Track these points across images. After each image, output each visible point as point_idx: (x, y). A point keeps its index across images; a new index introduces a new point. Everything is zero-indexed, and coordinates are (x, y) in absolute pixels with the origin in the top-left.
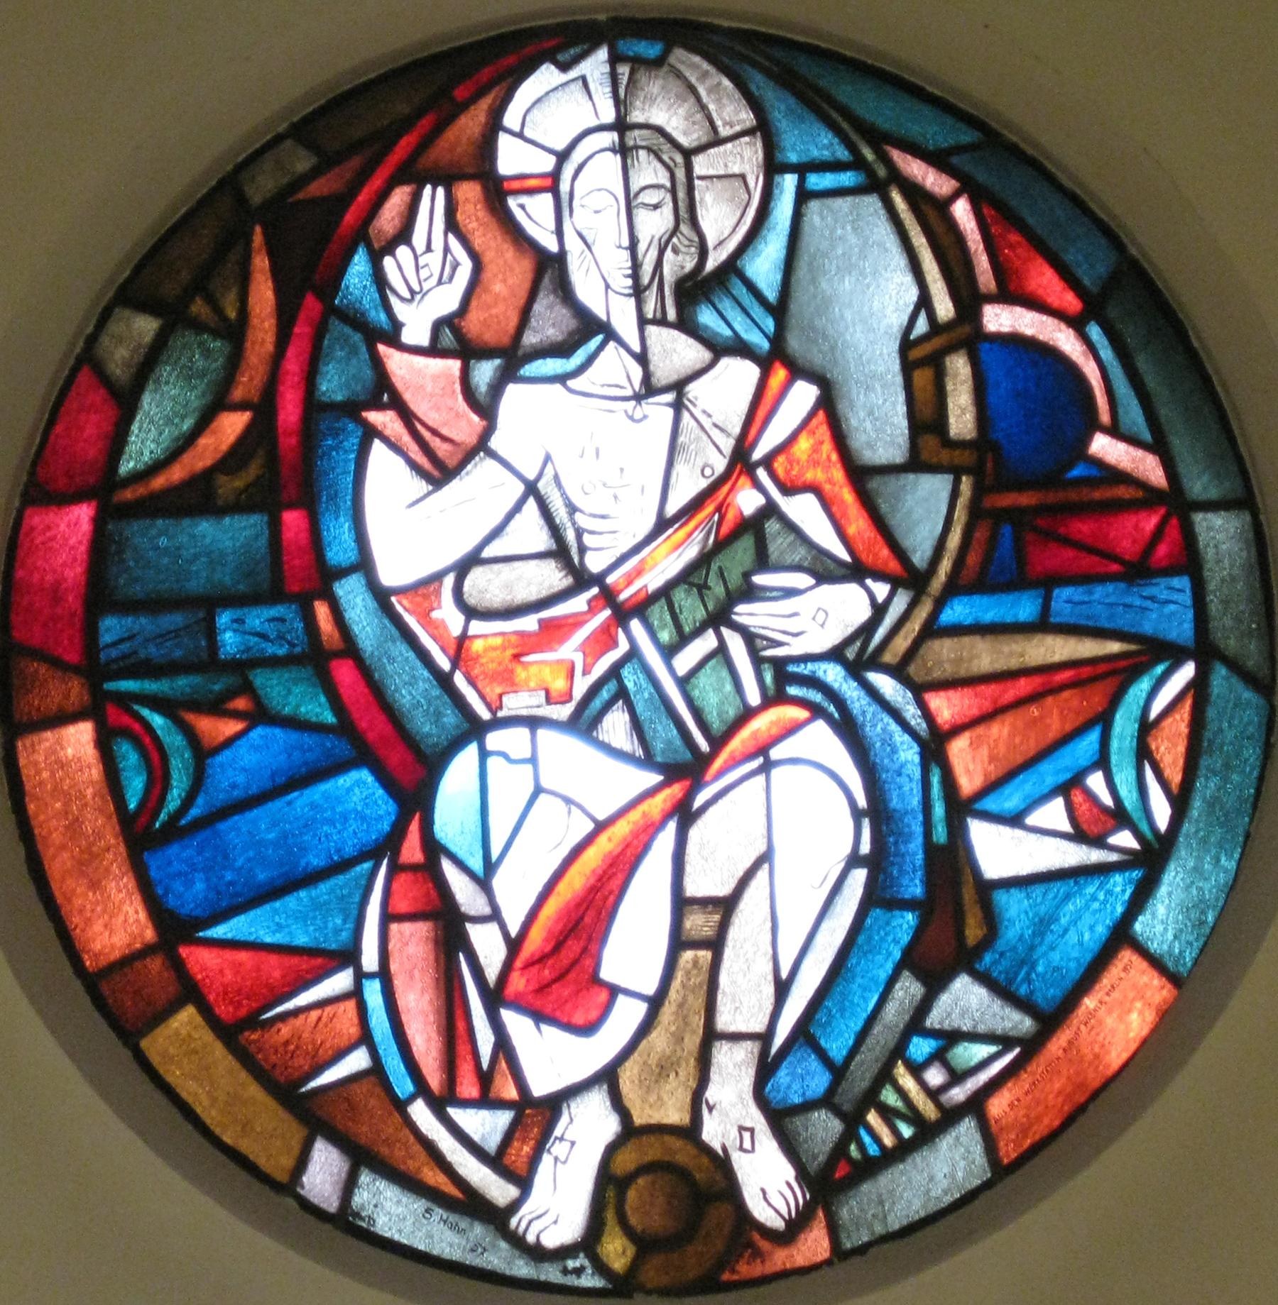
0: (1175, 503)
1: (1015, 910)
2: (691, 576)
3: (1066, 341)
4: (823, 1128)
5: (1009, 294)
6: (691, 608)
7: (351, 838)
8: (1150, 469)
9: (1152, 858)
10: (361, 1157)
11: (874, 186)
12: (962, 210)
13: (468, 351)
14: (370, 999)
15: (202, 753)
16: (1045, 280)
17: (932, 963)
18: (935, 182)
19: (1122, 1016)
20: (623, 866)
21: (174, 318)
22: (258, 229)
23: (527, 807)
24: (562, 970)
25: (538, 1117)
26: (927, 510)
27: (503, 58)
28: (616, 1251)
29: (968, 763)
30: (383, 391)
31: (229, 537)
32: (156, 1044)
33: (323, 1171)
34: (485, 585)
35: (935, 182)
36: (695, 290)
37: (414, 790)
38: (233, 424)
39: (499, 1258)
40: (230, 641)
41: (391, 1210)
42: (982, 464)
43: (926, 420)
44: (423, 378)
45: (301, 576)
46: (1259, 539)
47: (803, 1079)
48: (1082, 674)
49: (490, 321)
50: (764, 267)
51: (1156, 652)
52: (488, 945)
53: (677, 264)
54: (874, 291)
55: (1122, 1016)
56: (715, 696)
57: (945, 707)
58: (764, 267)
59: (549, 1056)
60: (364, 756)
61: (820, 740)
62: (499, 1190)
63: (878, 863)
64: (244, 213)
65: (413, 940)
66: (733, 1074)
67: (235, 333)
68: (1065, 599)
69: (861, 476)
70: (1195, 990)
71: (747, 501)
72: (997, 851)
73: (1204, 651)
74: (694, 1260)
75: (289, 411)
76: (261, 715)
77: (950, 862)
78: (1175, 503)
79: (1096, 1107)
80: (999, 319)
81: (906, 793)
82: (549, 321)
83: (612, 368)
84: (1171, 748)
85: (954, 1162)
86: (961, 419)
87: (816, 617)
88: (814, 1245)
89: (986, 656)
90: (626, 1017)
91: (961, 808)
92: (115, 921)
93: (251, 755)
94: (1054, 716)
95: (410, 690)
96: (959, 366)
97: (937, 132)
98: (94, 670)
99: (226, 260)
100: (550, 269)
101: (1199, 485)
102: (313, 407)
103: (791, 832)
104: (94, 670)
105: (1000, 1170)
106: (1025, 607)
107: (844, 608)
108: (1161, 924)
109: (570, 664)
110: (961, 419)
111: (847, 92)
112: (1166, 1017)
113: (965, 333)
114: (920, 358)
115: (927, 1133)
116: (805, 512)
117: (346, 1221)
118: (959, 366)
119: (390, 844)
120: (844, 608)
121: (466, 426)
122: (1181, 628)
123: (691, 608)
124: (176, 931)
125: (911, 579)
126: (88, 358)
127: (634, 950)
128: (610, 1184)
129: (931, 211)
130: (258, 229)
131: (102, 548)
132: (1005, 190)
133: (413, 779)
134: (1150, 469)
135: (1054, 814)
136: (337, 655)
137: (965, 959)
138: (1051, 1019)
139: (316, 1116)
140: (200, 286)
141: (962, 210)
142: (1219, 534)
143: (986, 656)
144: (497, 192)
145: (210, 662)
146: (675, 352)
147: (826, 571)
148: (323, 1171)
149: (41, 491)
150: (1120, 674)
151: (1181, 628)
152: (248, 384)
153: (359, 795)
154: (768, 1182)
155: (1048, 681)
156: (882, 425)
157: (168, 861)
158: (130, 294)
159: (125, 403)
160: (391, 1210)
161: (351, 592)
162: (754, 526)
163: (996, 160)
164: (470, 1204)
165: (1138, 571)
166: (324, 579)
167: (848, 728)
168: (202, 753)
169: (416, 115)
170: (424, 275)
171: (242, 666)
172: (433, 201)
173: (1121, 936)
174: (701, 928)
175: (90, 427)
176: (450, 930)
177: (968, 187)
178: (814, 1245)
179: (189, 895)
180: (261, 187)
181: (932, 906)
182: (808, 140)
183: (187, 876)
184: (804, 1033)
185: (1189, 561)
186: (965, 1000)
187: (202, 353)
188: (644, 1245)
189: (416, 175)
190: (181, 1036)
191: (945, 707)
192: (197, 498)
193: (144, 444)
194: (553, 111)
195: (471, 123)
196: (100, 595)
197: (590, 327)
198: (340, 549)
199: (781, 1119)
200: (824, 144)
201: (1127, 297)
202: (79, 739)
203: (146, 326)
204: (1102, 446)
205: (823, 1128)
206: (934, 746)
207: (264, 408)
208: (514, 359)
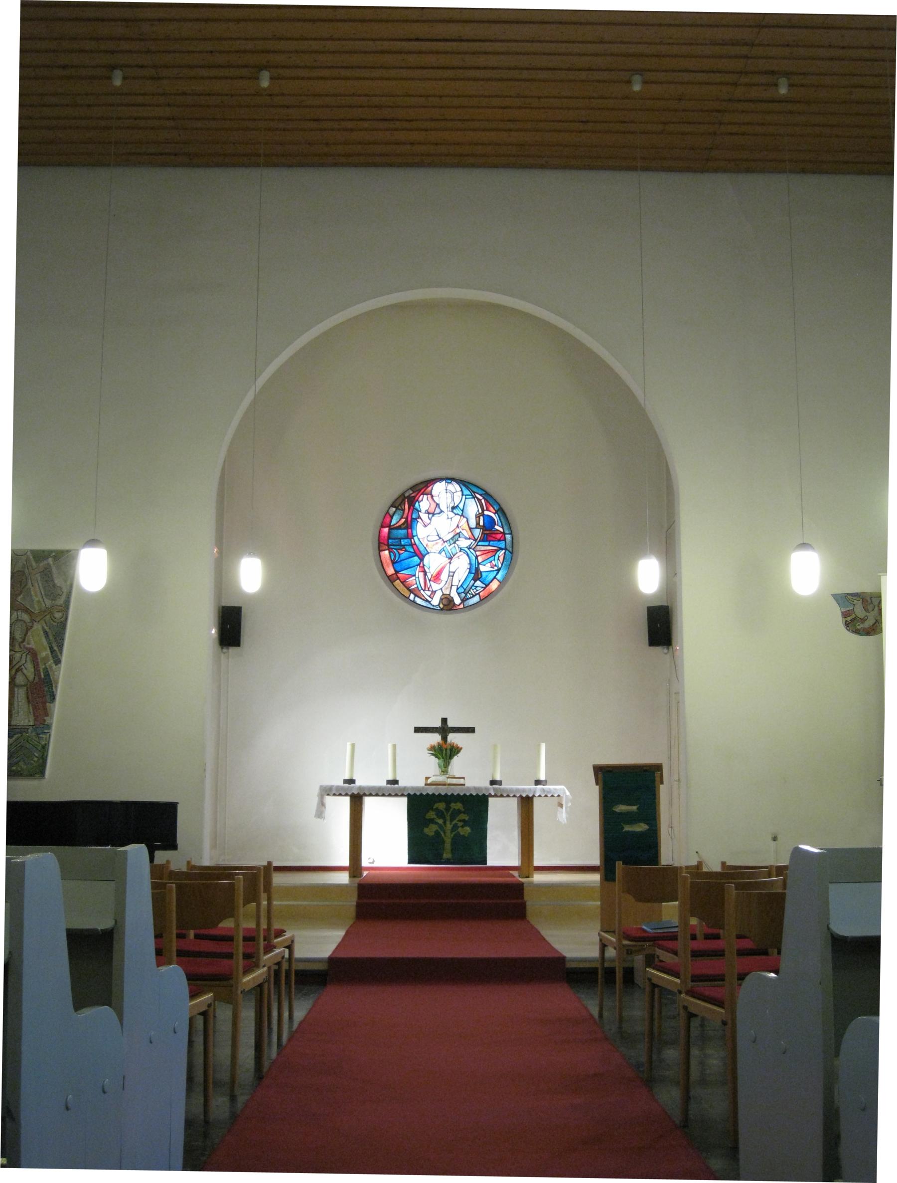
0: (504, 533)
1: (484, 574)
2: (452, 539)
3: (493, 515)
4: (463, 595)
5: (488, 510)
6: (452, 542)
7: (415, 564)
8: (501, 530)
9: (499, 570)
10: (416, 595)
11: (474, 497)
12: (483, 501)
13: (429, 513)
14: (417, 580)
15: (400, 554)
16: (491, 509)
17: (475, 579)
18: (480, 497)
19: (494, 585)
20: (443, 568)
21: (397, 508)
22: (543, 746)
23: (433, 562)
24: (437, 577)
25: (434, 592)
26: (477, 533)
27: (433, 481)
28: (441, 606)
29: (480, 559)
30: (419, 517)
31: (403, 532)
32: (395, 583)
33: (412, 597)
34: (429, 538)
35: (480, 497)
36: (453, 508)
37: (422, 559)
38: (403, 520)
39: (429, 606)
40: (403, 543)
41: (418, 600)
42: (484, 528)
43: (478, 524)
44: (424, 516)
45: (410, 536)
46: (512, 538)
47: (461, 590)
48: (492, 551)
49: (431, 510)
50: (461, 506)
51: (501, 549)
52: (429, 575)
53: (452, 505)
54: (472, 508)
55: (494, 585)
56: (454, 552)
57: (478, 553)
58: (461, 506)
59: (435, 586)
60: (417, 555)
61: (465, 556)
62: (430, 599)
63: (470, 569)
64: (405, 498)
65: (421, 574)
66: (454, 588)
67: (404, 510)
68: (491, 543)
69: (470, 529)
70: (502, 583)
71: (458, 531)
72: (482, 568)
73: (506, 549)
74: (450, 607)
75: (409, 519)
76: (406, 551)
77: (477, 569)
78: (504, 533)
79: (491, 595)
80: (486, 513)
81: (473, 562)
82: (438, 511)
83: (444, 516)
84: (501, 559)
85: (476, 599)
86: (481, 523)
87: (464, 543)
88: (462, 606)
89: (483, 548)
90: (443, 583)
91: (479, 564)
92: (391, 571)
93: (405, 555)
94: (490, 555)
95: (422, 549)
96: (482, 518)
97: (481, 492)
98: (388, 545)
99: (403, 502)
100: (438, 505)
101: (507, 532)
102: (412, 519)
103: (461, 566)
104: (388, 545)
105: (481, 600)
106: (487, 543)
107: (468, 542)
108: (499, 577)
109: (440, 546)
110: (481, 523)
111: (471, 487)
112: (499, 586)
113: (483, 515)
114: (477, 517)
115: (474, 596)
116: (464, 532)
117: (414, 602)
118: (482, 518)
119: (419, 565)
120: (468, 542)
121: (428, 521)
122: (503, 547)
123: (452, 542)
124: (397, 572)
125: (475, 540)
126: (388, 512)
127: (444, 576)
128: (441, 599)
129: (479, 500)
130: (543, 746)
131: (389, 533)
132: (488, 499)
133: (422, 557)
134: (501, 530)
135: (489, 565)
136: (445, 739)
137: (478, 579)
138: (487, 586)
139: (411, 591)
140: (400, 505)
141: (483, 501)
142: (508, 537)
143: (483, 548)
144: (432, 496)
145: (401, 545)
146: (451, 515)
147: (466, 538)
148: (412, 597)
149: (382, 526)
150: (497, 551)
151: (503, 547)
152: (405, 516)
153: (416, 559)
154: (457, 601)
155: (489, 551)
156: (473, 524)
157: (396, 565)
158: (392, 506)
159: (392, 517)
160: (418, 600)
161: (415, 538)
162: (459, 534)
163: (487, 495)
164: (427, 601)
165: (499, 540)
166: (413, 537)
167: (468, 555)
168: (400, 554)
169: (423, 487)
170: (424, 504)
171: (404, 546)
172: (425, 496)
173: (495, 578)
174: (452, 575)
175: (388, 520)
176: (425, 574)
177: (485, 500)
178: (462, 606)
179: (398, 569)
180: (407, 495)
181: (476, 575)
182: (466, 492)
183: (397, 566)
184: (461, 586)
185: (505, 540)
186: (478, 583)
187: (400, 512)
188: (444, 605)
189: (423, 494)
190: (397, 582)
191: (478, 553)
192: (399, 528)
193: (394, 522)
194: (439, 488)
195: (430, 488)
196: (389, 538)
197: (442, 511)
198: (414, 534)
199: (459, 594)
200: (468, 493)
201: (501, 511)
202: (387, 552)
203: (394, 509)
204: (497, 527)
205: (463, 595)
206: (477, 557)
207: (407, 519)
208: (433, 514)
